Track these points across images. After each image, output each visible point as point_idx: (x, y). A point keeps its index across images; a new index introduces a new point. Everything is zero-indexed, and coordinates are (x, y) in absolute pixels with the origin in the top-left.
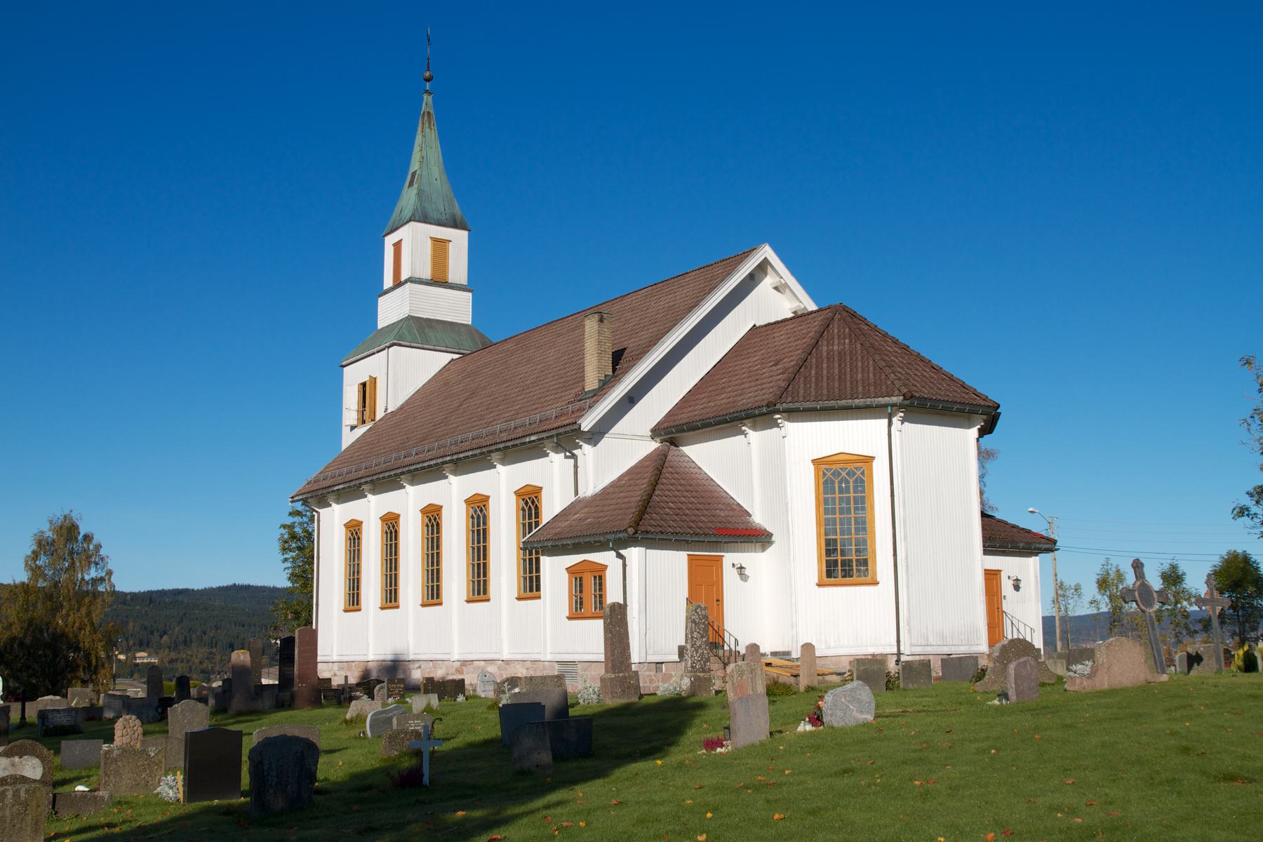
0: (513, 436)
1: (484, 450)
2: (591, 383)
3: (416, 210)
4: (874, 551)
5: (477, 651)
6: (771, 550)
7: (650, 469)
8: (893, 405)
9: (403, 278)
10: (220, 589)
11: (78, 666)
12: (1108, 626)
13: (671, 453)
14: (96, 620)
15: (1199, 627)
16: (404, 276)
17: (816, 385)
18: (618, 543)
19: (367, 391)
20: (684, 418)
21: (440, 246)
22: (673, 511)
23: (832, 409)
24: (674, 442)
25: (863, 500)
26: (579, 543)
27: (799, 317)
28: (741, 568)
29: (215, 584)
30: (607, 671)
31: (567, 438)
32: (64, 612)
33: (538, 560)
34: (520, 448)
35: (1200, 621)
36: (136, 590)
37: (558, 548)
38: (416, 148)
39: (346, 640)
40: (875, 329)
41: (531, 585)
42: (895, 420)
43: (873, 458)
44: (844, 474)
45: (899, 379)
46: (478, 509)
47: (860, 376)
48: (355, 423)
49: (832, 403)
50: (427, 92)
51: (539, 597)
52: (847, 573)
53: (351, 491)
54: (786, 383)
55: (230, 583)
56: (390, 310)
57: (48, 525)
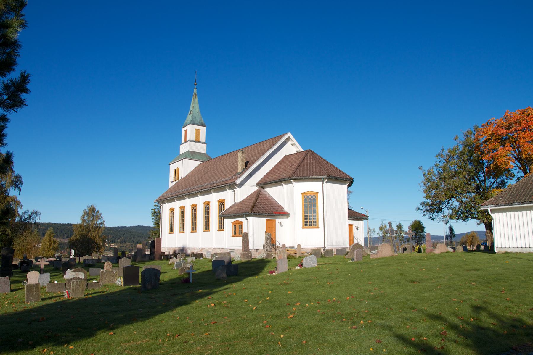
2: (240, 170)
6: (289, 218)
14: (100, 235)
15: (406, 240)
18: (246, 216)
19: (176, 171)
20: (265, 181)
21: (198, 131)
22: (261, 207)
23: (297, 179)
24: (262, 187)
27: (298, 153)
31: (232, 186)
34: (219, 188)
37: (229, 217)
38: (192, 104)
39: (169, 242)
40: (319, 157)
41: (222, 227)
46: (207, 206)
52: (310, 225)
56: (183, 149)
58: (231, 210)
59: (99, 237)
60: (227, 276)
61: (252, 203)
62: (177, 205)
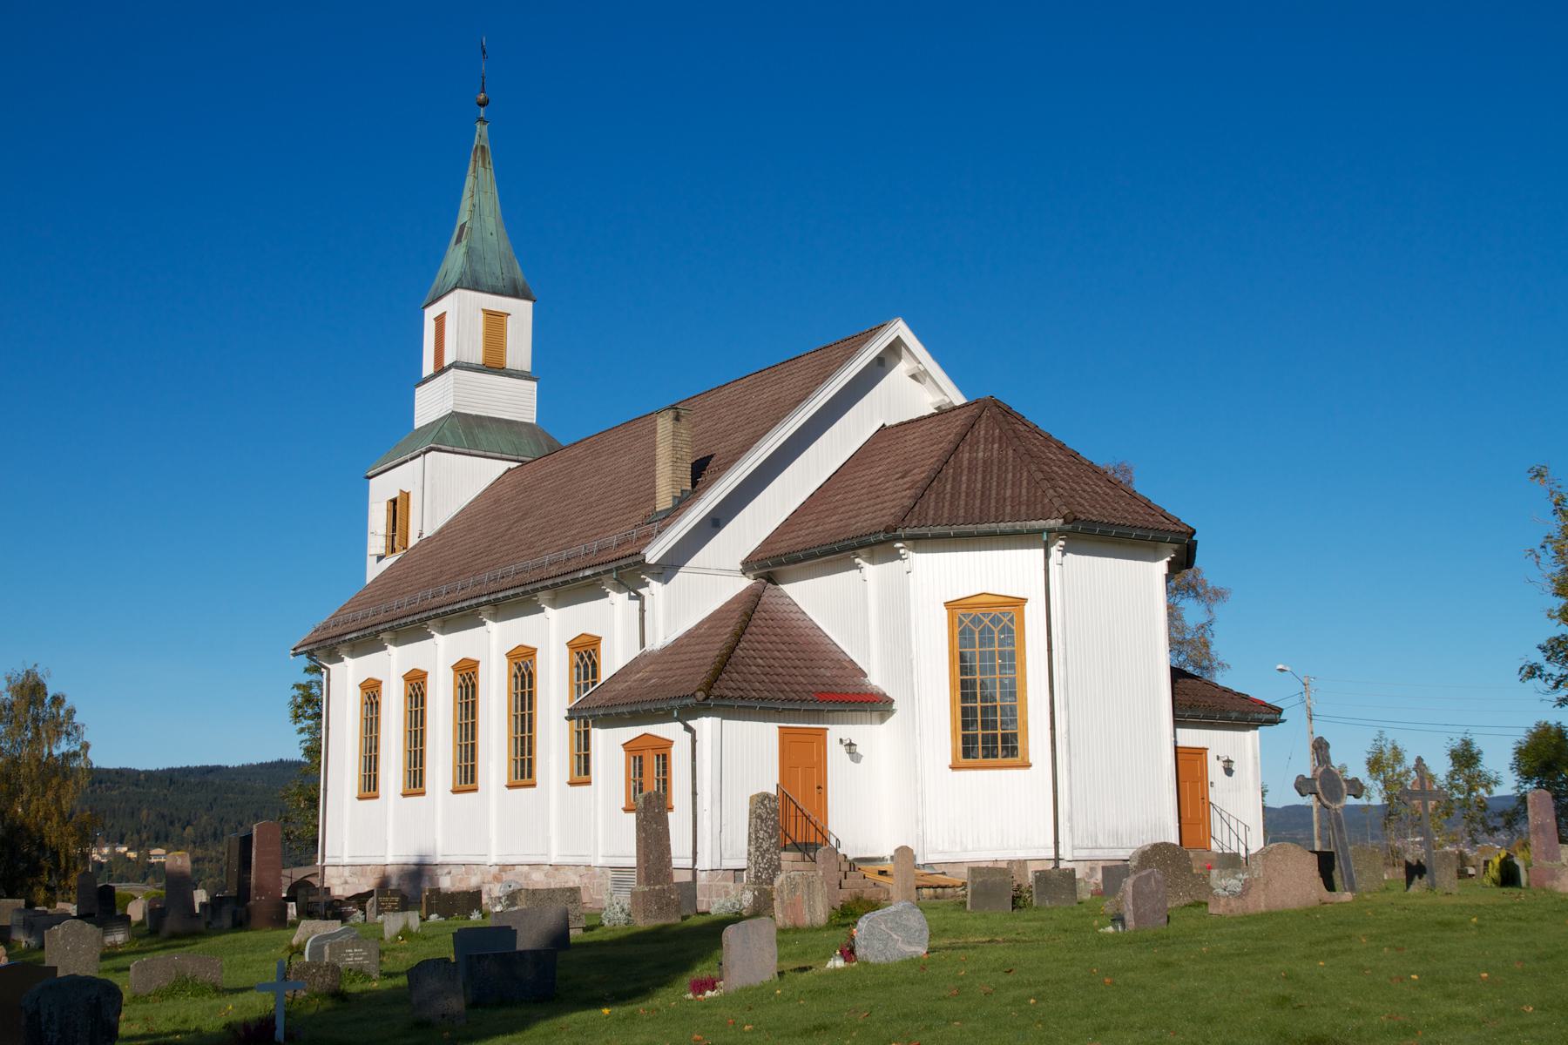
0: (563, 570)
1: (529, 588)
2: (664, 501)
3: (463, 274)
4: (1026, 723)
5: (519, 853)
6: (891, 721)
7: (737, 615)
8: (1050, 531)
9: (447, 363)
10: (262, 765)
11: (41, 869)
12: (1382, 820)
13: (766, 594)
14: (66, 807)
15: (1500, 822)
16: (448, 360)
17: (951, 504)
18: (686, 712)
19: (397, 509)
20: (783, 547)
21: (495, 321)
22: (765, 670)
23: (970, 535)
24: (771, 579)
25: (1012, 656)
26: (637, 712)
27: (942, 413)
28: (851, 744)
29: (255, 759)
30: (639, 883)
31: (629, 573)
32: (25, 797)
33: (587, 734)
34: (574, 586)
35: (1501, 815)
36: (152, 767)
37: (612, 718)
38: (466, 193)
39: (361, 837)
40: (1035, 430)
41: (582, 770)
42: (1054, 550)
43: (1024, 600)
44: (986, 621)
45: (1060, 496)
46: (523, 668)
47: (1009, 493)
48: (383, 551)
49: (970, 528)
50: (480, 119)
51: (589, 783)
52: (990, 753)
53: (366, 641)
54: (912, 502)
55: (275, 759)
56: (430, 404)
57: (5, 684)
58: (620, 687)
59: (65, 819)
60: (473, 1005)
61: (714, 651)
62: (391, 664)
